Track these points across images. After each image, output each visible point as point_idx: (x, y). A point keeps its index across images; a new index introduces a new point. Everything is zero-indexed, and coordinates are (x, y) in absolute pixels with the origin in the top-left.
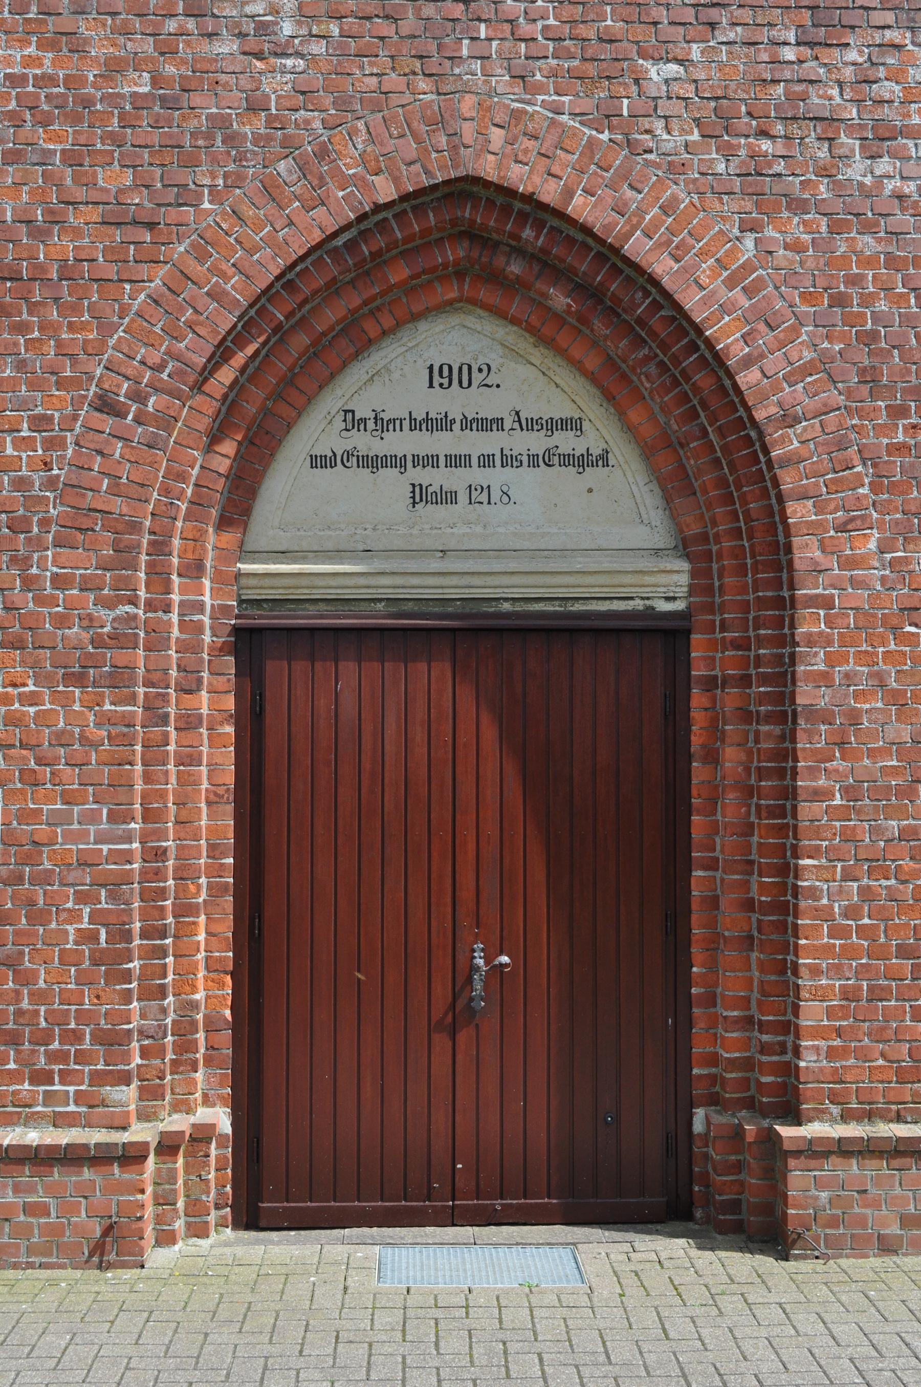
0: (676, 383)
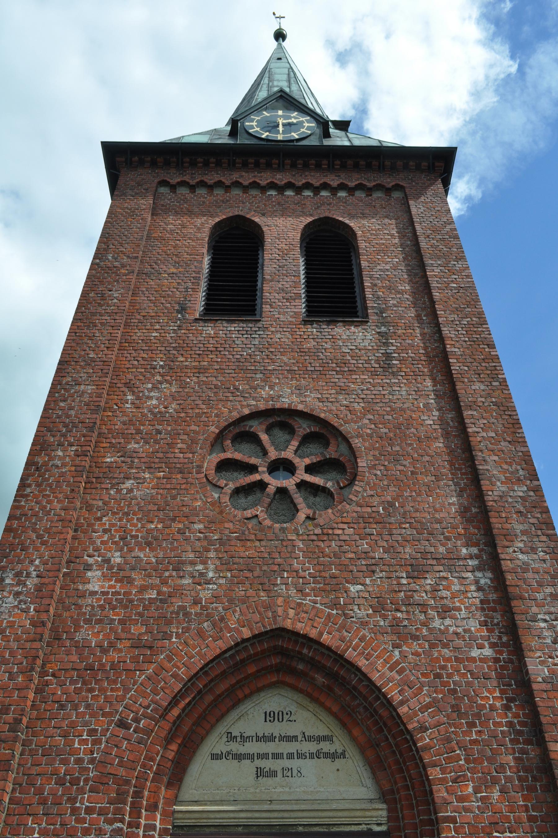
0: (372, 716)
